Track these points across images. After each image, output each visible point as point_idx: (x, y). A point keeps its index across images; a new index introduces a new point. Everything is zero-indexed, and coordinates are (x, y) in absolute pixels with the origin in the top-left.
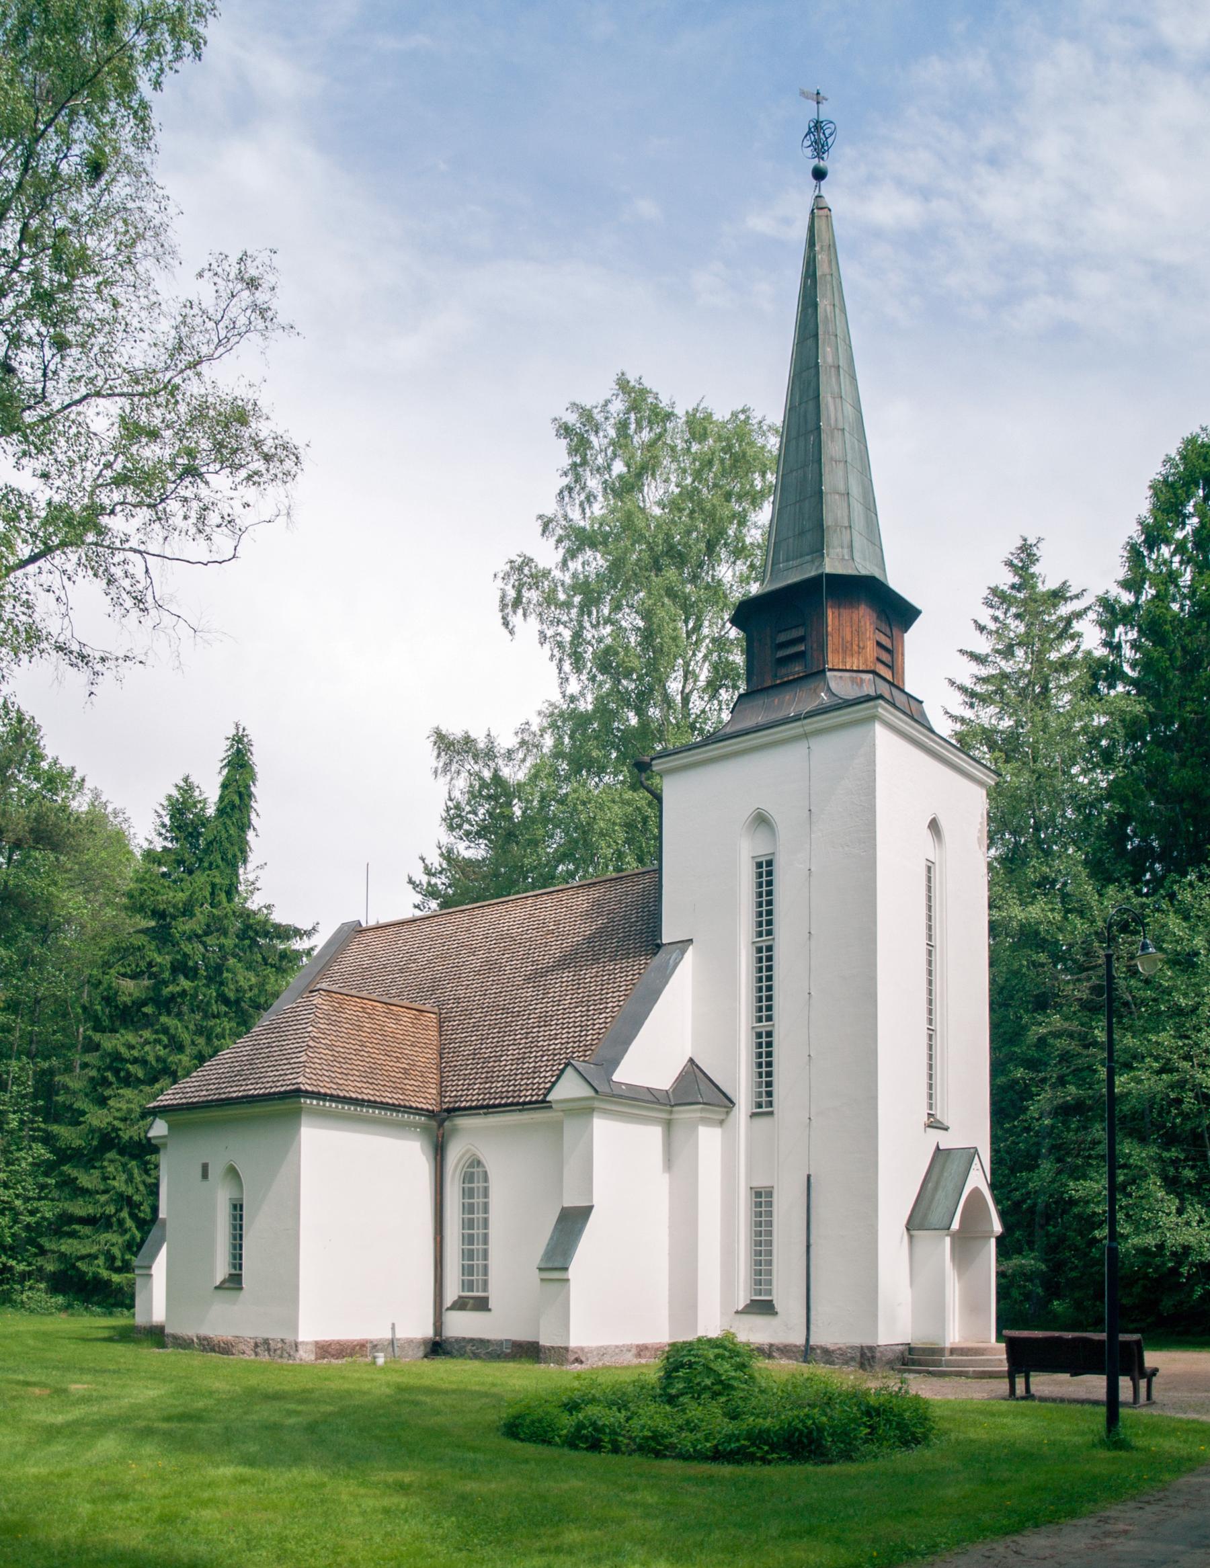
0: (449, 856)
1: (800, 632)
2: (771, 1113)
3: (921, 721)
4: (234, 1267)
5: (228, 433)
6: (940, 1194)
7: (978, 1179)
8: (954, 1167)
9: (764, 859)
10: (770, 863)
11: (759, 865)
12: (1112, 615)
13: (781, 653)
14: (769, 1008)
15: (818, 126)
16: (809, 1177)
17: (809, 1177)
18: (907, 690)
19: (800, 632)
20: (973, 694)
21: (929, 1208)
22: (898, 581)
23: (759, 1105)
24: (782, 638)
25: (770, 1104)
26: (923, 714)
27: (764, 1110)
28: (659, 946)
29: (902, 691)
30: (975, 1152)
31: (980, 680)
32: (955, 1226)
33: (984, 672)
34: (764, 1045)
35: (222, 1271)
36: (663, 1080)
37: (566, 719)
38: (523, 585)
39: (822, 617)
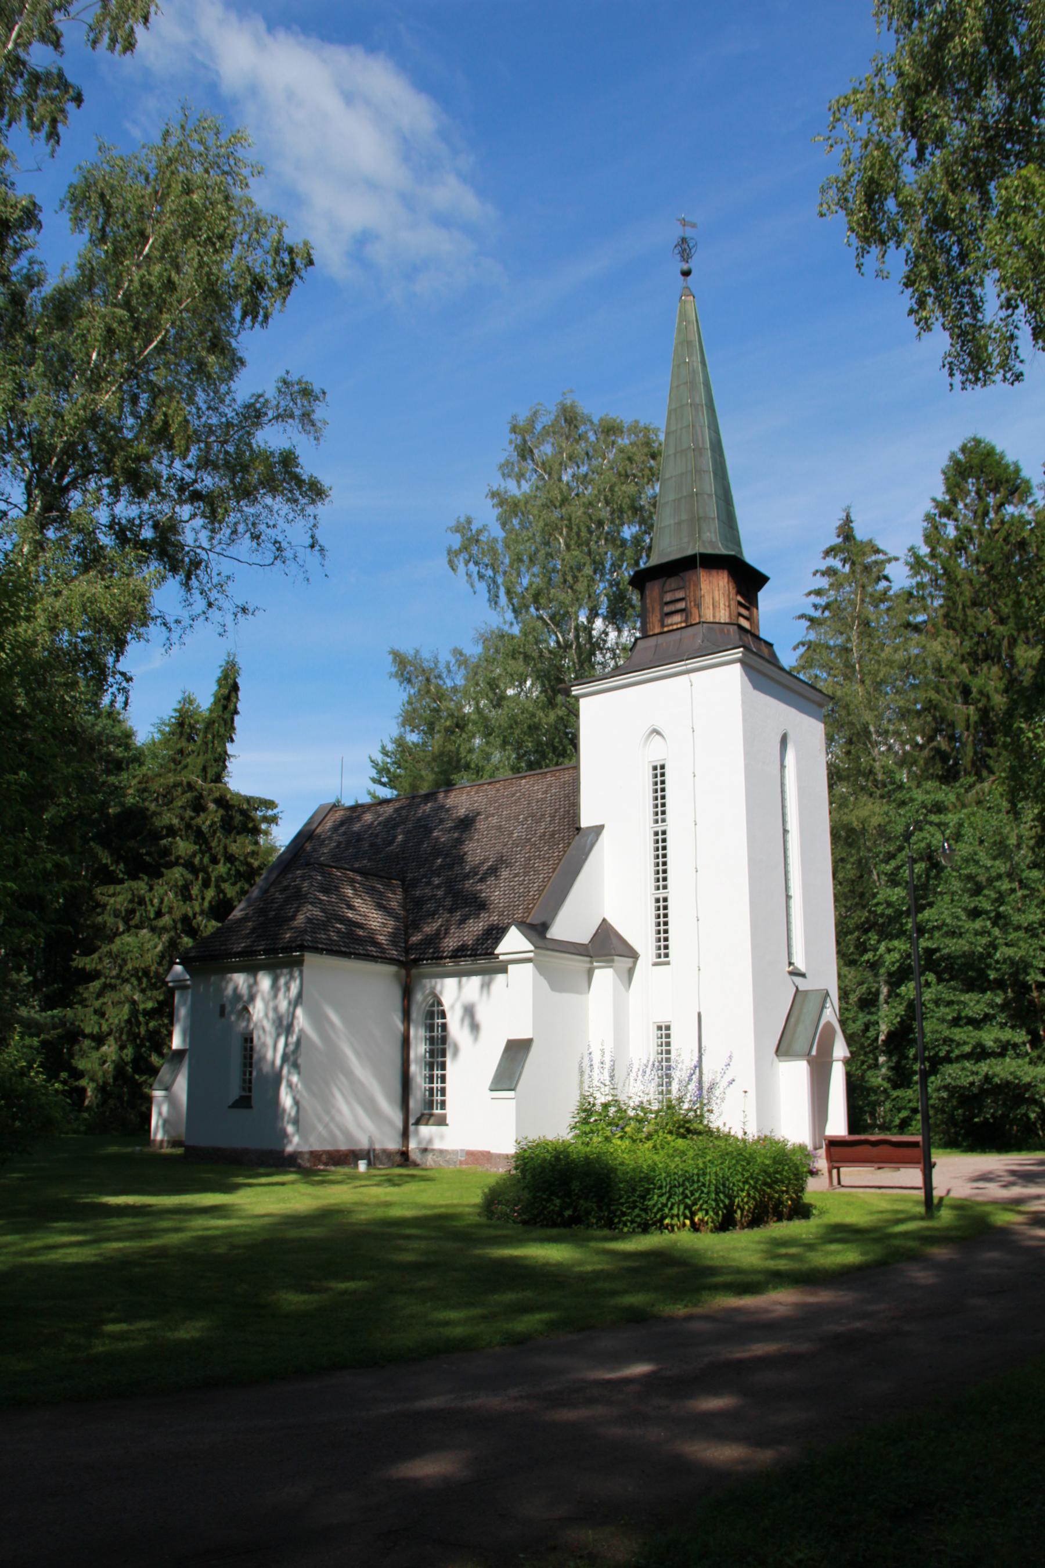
0: (400, 742)
1: (680, 594)
2: (668, 963)
3: (773, 660)
4: (244, 1089)
5: (285, 476)
6: (801, 1028)
7: (830, 1015)
8: (812, 1006)
9: (658, 764)
10: (663, 767)
11: (655, 768)
12: (917, 564)
13: (667, 609)
14: (665, 879)
15: (684, 240)
16: (699, 1015)
17: (699, 1015)
18: (762, 636)
19: (680, 594)
20: (811, 620)
21: (250, 1185)
22: (751, 556)
23: (659, 956)
24: (668, 597)
25: (667, 955)
26: (773, 655)
27: (663, 959)
28: (579, 829)
29: (757, 638)
30: (827, 994)
31: (816, 606)
32: (814, 1052)
33: (822, 601)
34: (662, 907)
35: (235, 1092)
36: (583, 936)
37: (498, 644)
38: (469, 544)
39: (697, 584)
